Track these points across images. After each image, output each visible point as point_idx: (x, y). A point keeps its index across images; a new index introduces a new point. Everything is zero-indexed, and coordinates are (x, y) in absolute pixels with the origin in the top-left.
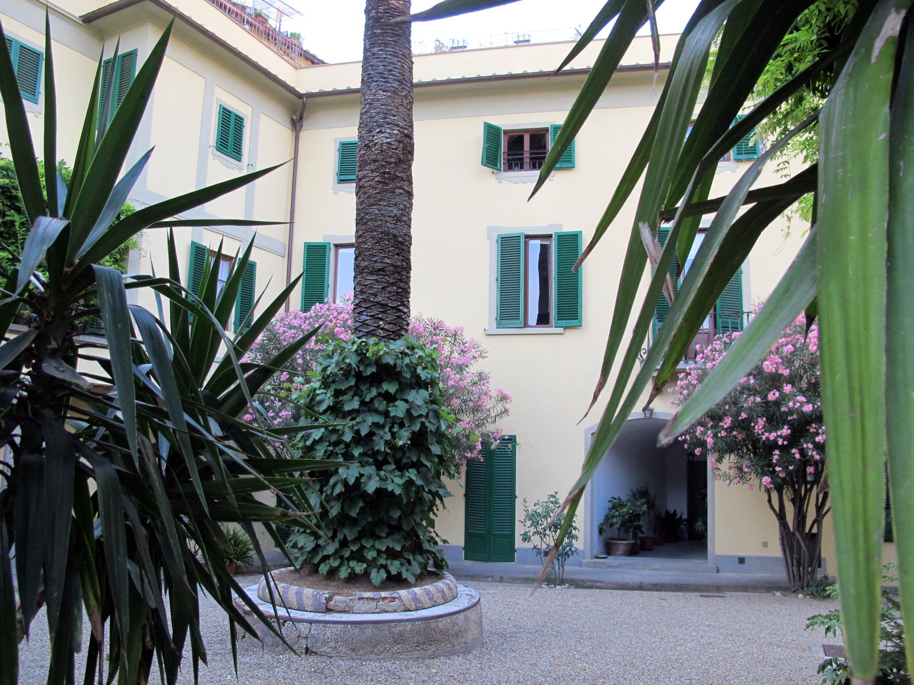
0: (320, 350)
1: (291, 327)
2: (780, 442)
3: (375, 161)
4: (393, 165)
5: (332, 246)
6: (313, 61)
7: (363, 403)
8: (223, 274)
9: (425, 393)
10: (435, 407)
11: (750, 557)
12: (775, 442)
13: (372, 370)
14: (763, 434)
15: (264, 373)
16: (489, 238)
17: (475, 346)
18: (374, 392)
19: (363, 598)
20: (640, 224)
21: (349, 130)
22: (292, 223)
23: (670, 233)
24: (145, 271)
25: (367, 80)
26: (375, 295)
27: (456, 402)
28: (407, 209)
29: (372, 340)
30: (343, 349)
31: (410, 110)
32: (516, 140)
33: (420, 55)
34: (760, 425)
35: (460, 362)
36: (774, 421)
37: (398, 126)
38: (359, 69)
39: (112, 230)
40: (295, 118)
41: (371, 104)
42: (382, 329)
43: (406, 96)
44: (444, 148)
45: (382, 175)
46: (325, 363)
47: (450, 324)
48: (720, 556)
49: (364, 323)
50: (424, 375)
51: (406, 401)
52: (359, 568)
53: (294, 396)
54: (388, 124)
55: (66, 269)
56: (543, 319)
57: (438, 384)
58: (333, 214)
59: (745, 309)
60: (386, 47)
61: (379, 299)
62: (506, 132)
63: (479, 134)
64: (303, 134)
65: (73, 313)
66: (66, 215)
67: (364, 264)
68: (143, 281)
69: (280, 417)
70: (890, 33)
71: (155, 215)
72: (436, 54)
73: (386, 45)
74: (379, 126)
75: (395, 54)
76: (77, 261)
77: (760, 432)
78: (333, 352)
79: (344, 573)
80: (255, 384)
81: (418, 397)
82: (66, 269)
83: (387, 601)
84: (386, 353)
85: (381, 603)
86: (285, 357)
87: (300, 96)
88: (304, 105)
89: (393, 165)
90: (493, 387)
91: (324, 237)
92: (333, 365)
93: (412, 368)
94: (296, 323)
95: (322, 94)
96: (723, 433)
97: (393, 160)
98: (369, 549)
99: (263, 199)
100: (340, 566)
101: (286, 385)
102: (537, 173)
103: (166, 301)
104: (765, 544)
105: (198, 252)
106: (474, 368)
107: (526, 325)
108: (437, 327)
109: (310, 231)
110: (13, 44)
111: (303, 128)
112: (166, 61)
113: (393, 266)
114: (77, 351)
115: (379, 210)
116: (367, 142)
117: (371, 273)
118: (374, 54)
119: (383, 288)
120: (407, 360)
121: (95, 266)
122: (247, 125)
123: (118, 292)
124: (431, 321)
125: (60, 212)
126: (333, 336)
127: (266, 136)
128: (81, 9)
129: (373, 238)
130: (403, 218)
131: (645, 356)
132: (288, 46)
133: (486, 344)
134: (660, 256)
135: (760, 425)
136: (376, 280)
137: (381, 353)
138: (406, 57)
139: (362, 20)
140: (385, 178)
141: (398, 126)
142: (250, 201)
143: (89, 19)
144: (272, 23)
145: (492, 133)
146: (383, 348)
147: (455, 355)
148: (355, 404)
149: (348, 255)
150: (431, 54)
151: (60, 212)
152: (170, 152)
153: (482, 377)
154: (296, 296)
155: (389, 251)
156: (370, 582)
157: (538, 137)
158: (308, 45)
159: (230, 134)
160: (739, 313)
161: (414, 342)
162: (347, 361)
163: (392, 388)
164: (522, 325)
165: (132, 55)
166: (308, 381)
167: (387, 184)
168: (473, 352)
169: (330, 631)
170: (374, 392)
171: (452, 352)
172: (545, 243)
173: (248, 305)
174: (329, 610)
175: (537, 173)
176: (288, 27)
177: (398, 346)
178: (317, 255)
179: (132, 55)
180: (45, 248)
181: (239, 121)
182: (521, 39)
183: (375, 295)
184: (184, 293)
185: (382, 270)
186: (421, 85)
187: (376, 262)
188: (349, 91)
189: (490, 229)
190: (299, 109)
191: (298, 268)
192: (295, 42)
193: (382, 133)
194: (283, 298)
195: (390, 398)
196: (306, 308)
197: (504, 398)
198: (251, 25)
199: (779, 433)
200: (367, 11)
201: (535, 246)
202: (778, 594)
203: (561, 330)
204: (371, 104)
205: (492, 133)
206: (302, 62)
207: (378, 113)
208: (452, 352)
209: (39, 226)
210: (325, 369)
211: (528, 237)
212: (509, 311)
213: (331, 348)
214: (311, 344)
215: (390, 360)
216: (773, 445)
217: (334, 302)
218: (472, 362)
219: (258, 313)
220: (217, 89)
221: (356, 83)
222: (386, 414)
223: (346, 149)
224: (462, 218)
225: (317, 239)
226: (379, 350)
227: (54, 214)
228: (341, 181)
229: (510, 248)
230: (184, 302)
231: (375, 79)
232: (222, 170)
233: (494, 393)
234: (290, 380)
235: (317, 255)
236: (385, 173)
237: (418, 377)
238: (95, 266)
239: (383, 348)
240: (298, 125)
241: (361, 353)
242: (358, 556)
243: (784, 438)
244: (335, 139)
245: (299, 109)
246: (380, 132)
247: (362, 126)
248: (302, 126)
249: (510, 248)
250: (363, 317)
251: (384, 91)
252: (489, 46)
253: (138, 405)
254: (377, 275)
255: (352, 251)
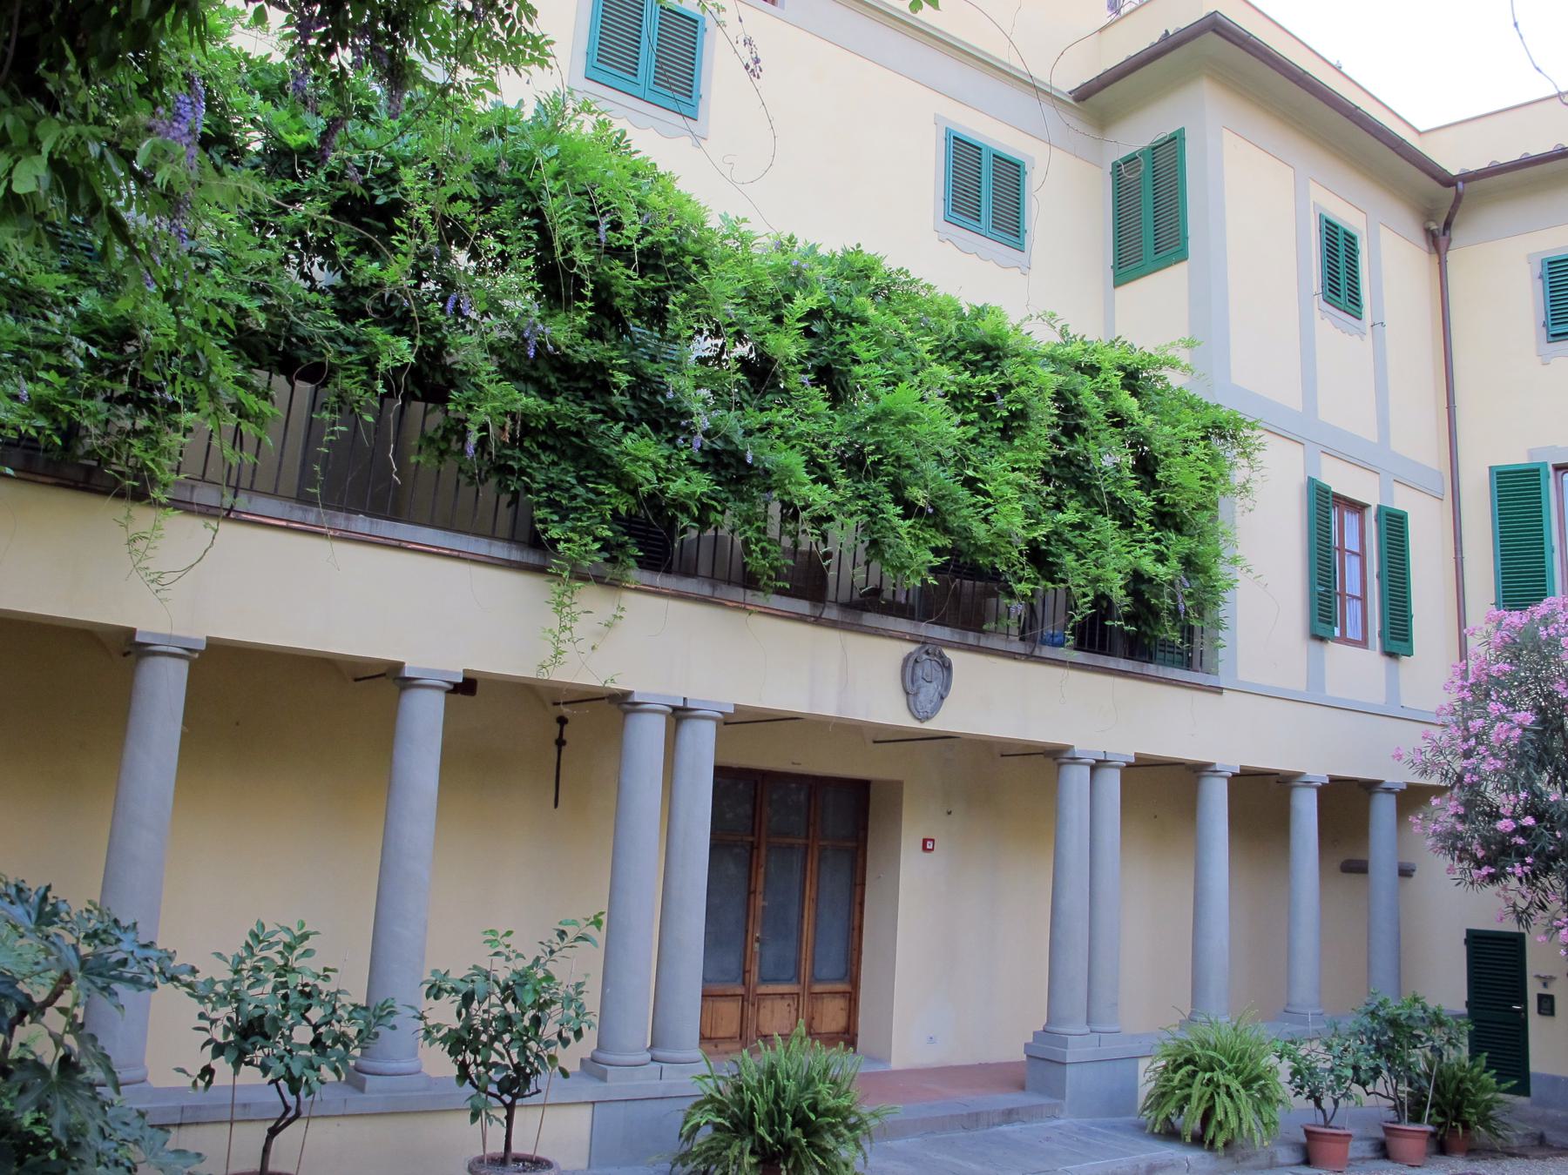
5: (1551, 469)
23: (880, 1068)
40: (1433, 226)
64: (1450, 256)
70: (367, 524)
87: (1448, 181)
88: (1458, 198)
91: (1530, 453)
110: (984, 152)
111: (1452, 245)
122: (1363, 246)
128: (1069, 79)
143: (1084, 94)
177: (839, 1060)
181: (1351, 239)
220: (1313, 186)
225: (1515, 457)
228: (1556, 336)
240: (1442, 240)
244: (1529, 256)
248: (1450, 240)
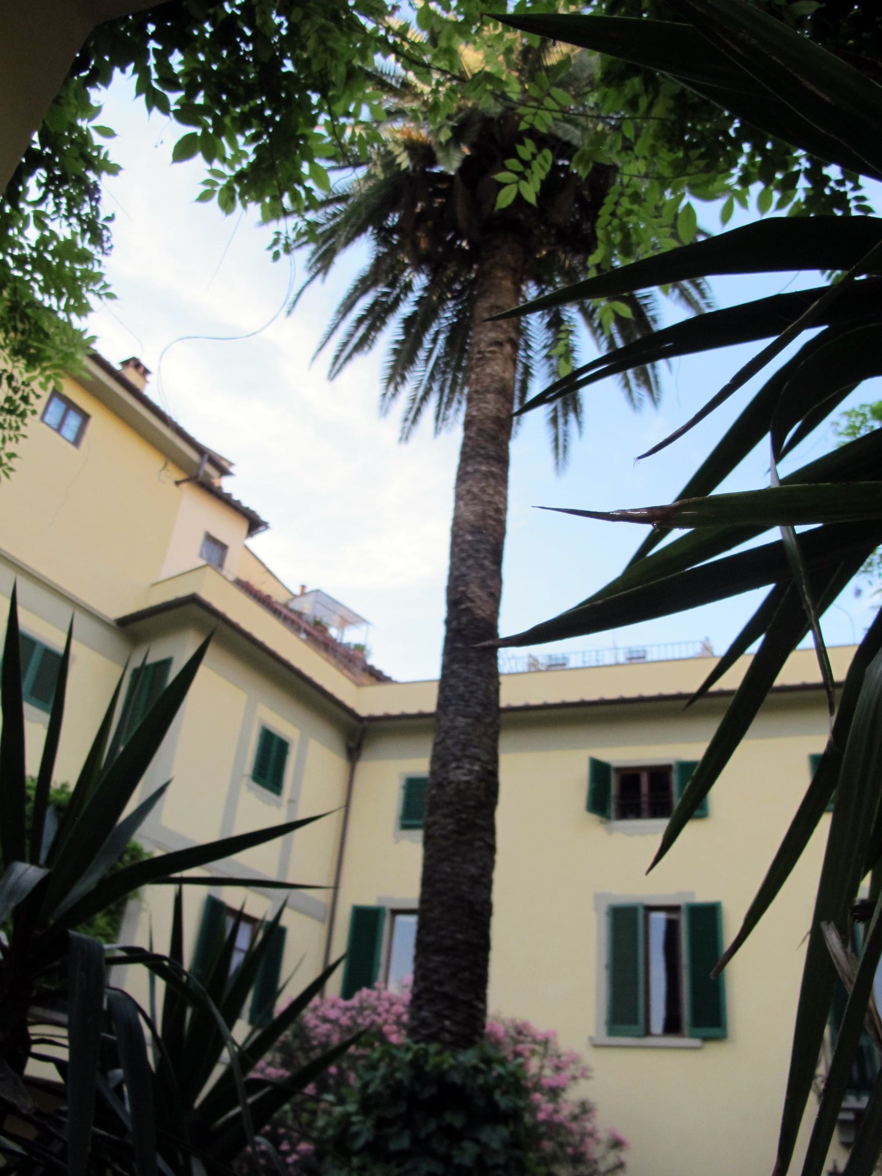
0: (361, 1057)
1: (325, 1020)
6: (377, 677)
7: (415, 1141)
8: (243, 940)
9: (503, 1132)
10: (518, 1153)
13: (430, 1092)
15: (281, 1092)
16: (597, 909)
17: (575, 1059)
18: (432, 1125)
20: (823, 925)
21: (419, 764)
22: (336, 888)
24: (141, 941)
25: (444, 701)
27: (548, 1146)
28: (488, 867)
29: (433, 1048)
30: (393, 1058)
31: (495, 740)
32: (630, 777)
33: (509, 674)
35: (554, 1083)
37: (479, 760)
38: (434, 691)
39: (103, 883)
42: (449, 1032)
43: (491, 724)
44: (538, 792)
45: (456, 822)
46: (367, 1076)
47: (540, 1025)
49: (424, 1023)
50: (503, 1102)
51: (477, 1141)
53: (321, 1122)
55: (37, 932)
56: (672, 1026)
57: (522, 1117)
58: (392, 869)
61: (446, 988)
62: (619, 770)
63: (582, 773)
65: (34, 993)
66: (48, 864)
67: (430, 939)
68: (135, 955)
69: (298, 1153)
71: (164, 869)
72: (529, 672)
73: (468, 661)
75: (479, 673)
76: (52, 922)
78: (380, 1060)
80: (263, 1113)
81: (495, 1137)
82: (37, 932)
84: (452, 1067)
86: (314, 1071)
90: (603, 1123)
92: (377, 1081)
93: (487, 1091)
94: (333, 1014)
95: (388, 718)
97: (472, 803)
99: (303, 858)
101: (310, 1105)
102: (662, 824)
103: (161, 984)
105: (215, 910)
106: (574, 1094)
107: (647, 1033)
108: (521, 1031)
109: (359, 892)
112: (203, 671)
114: (29, 1048)
116: (440, 779)
120: (480, 1080)
121: (72, 932)
123: (98, 966)
124: (513, 1021)
125: (44, 854)
126: (382, 1037)
127: (315, 762)
130: (483, 881)
131: (822, 1086)
132: (352, 660)
133: (590, 1057)
134: (856, 972)
137: (446, 1066)
138: (492, 676)
139: (441, 632)
141: (479, 760)
142: (284, 862)
144: (333, 632)
145: (600, 772)
146: (449, 1061)
147: (548, 1072)
148: (404, 1142)
149: (407, 926)
150: (523, 673)
151: (44, 854)
152: (194, 790)
153: (585, 1109)
154: (335, 984)
157: (659, 775)
158: (375, 660)
159: (271, 764)
160: (467, 425)
161: (491, 1052)
162: (398, 1075)
163: (457, 1120)
164: (642, 1032)
165: (166, 664)
166: (341, 1101)
168: (572, 1070)
170: (432, 1125)
171: (542, 1068)
172: (673, 916)
173: (270, 991)
175: (662, 824)
176: (350, 637)
177: (469, 1057)
178: (368, 924)
179: (166, 664)
180: (12, 905)
182: (635, 655)
183: (441, 983)
184: (185, 978)
186: (511, 709)
188: (421, 716)
189: (598, 897)
190: (358, 736)
191: (340, 947)
192: (358, 654)
194: (317, 986)
195: (454, 1136)
196: (348, 992)
197: (617, 1144)
198: (308, 633)
200: (448, 622)
201: (658, 920)
203: (696, 1042)
205: (600, 772)
206: (365, 678)
208: (542, 1068)
209: (10, 875)
210: (366, 1085)
211: (650, 909)
212: (624, 1012)
213: (376, 1055)
214: (352, 1049)
215: (456, 1078)
217: (386, 988)
218: (572, 1083)
219: (282, 1004)
221: (429, 705)
222: (447, 1160)
223: (413, 786)
224: (559, 879)
225: (369, 900)
226: (442, 1063)
227: (34, 861)
229: (625, 924)
230: (184, 987)
231: (454, 702)
232: (257, 811)
233: (603, 1135)
234: (317, 1099)
235: (368, 924)
236: (461, 819)
237: (494, 1105)
238: (72, 932)
239: (449, 1061)
241: (417, 1064)
245: (358, 736)
246: (458, 768)
247: (436, 759)
249: (625, 924)
250: (425, 1014)
252: (593, 664)
253: (95, 1135)
255: (413, 920)
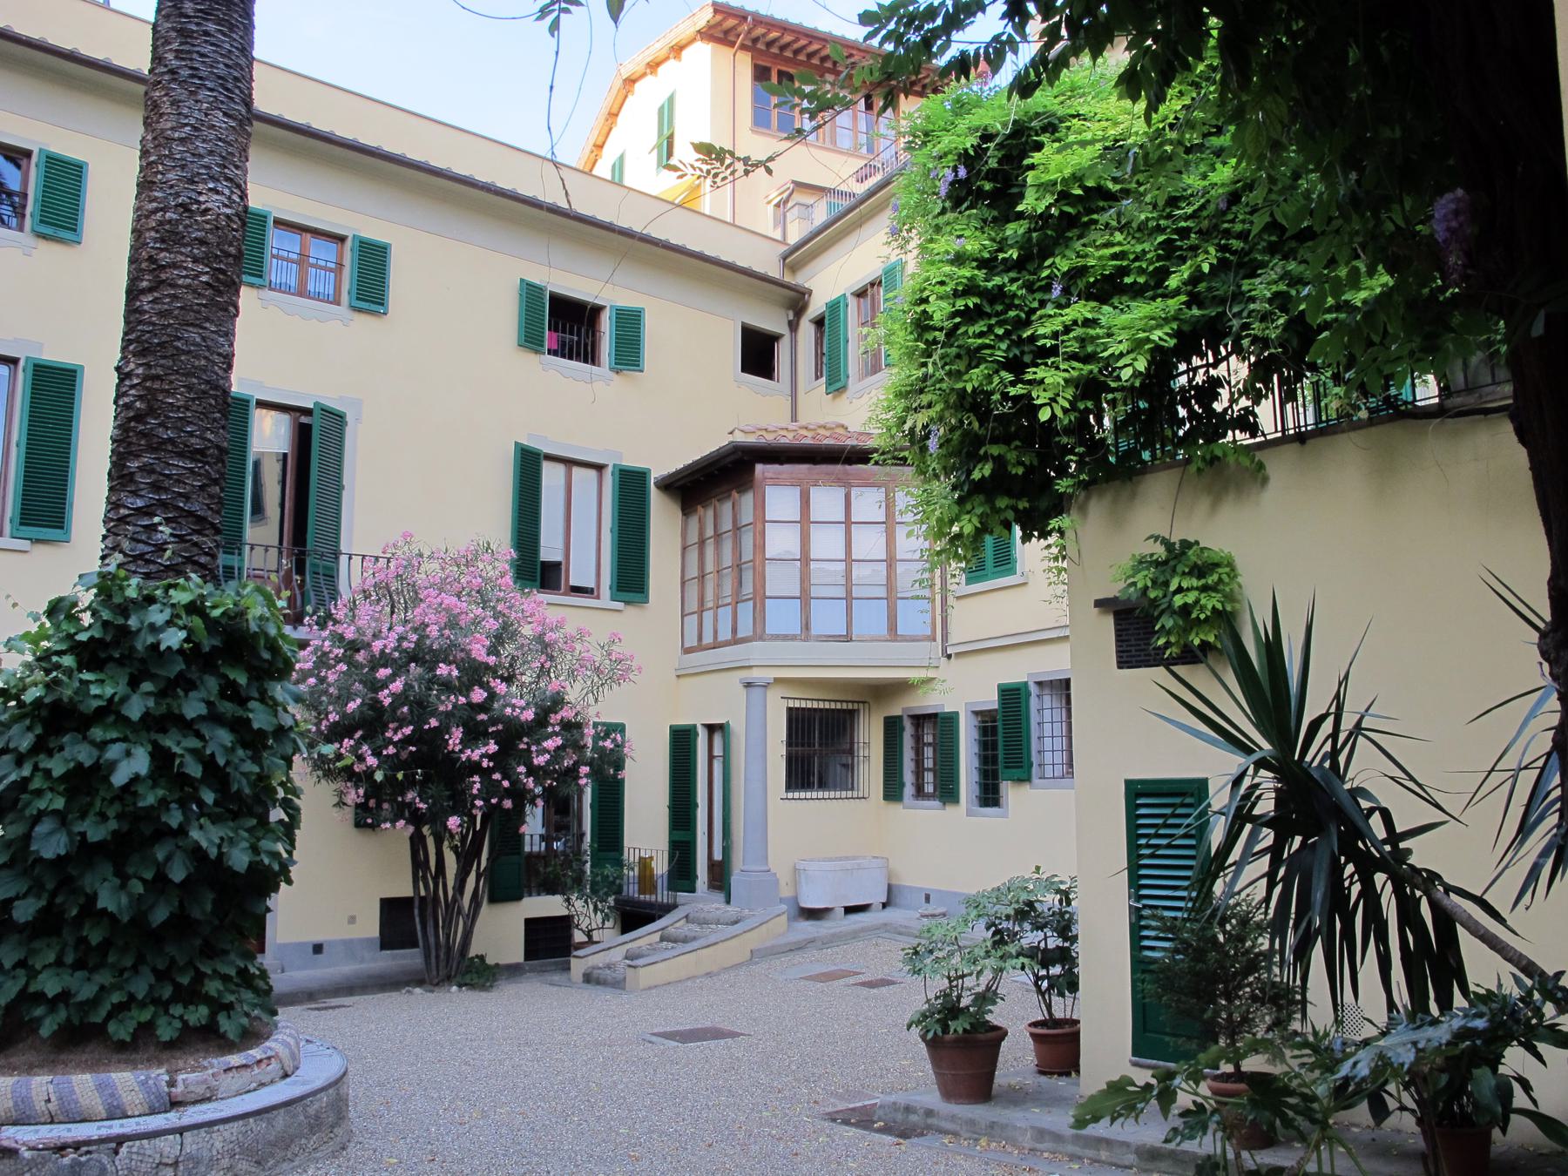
2: (485, 764)
3: (202, 242)
4: (231, 260)
11: (330, 942)
12: (478, 764)
14: (461, 751)
19: (230, 1069)
26: (186, 497)
34: (455, 738)
36: (475, 734)
41: (195, 129)
48: (285, 945)
52: (198, 1015)
54: (228, 179)
59: (343, 548)
60: (231, 30)
74: (213, 178)
77: (457, 749)
79: (166, 1032)
83: (263, 1066)
85: (256, 1070)
89: (231, 260)
96: (391, 750)
98: (211, 978)
100: (155, 1016)
104: (352, 920)
113: (218, 447)
115: (204, 339)
117: (180, 455)
118: (206, 33)
119: (202, 488)
129: (190, 388)
135: (455, 738)
136: (190, 469)
140: (218, 280)
155: (215, 420)
156: (223, 1036)
167: (220, 293)
169: (219, 1140)
174: (175, 1104)
183: (186, 497)
185: (202, 452)
187: (191, 434)
193: (217, 192)
199: (483, 750)
202: (418, 990)
204: (195, 129)
207: (211, 153)
216: (474, 768)
242: (191, 995)
243: (491, 757)
251: (225, 114)
254: (193, 460)
